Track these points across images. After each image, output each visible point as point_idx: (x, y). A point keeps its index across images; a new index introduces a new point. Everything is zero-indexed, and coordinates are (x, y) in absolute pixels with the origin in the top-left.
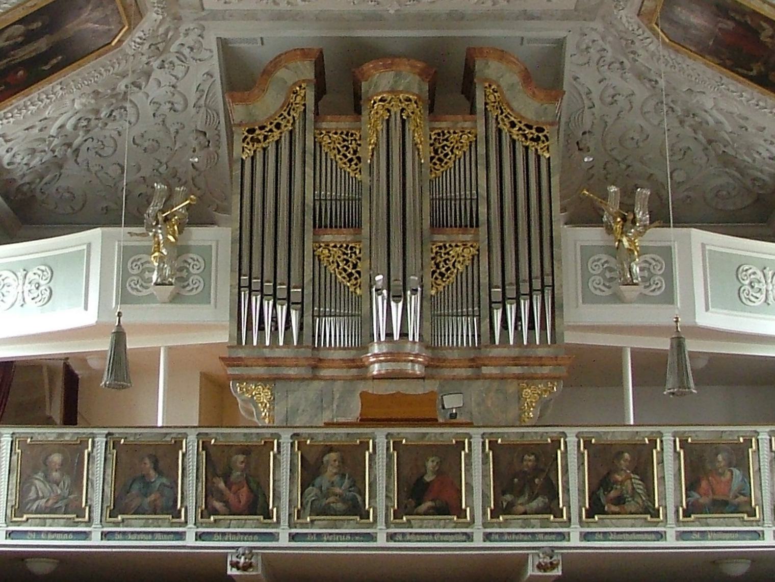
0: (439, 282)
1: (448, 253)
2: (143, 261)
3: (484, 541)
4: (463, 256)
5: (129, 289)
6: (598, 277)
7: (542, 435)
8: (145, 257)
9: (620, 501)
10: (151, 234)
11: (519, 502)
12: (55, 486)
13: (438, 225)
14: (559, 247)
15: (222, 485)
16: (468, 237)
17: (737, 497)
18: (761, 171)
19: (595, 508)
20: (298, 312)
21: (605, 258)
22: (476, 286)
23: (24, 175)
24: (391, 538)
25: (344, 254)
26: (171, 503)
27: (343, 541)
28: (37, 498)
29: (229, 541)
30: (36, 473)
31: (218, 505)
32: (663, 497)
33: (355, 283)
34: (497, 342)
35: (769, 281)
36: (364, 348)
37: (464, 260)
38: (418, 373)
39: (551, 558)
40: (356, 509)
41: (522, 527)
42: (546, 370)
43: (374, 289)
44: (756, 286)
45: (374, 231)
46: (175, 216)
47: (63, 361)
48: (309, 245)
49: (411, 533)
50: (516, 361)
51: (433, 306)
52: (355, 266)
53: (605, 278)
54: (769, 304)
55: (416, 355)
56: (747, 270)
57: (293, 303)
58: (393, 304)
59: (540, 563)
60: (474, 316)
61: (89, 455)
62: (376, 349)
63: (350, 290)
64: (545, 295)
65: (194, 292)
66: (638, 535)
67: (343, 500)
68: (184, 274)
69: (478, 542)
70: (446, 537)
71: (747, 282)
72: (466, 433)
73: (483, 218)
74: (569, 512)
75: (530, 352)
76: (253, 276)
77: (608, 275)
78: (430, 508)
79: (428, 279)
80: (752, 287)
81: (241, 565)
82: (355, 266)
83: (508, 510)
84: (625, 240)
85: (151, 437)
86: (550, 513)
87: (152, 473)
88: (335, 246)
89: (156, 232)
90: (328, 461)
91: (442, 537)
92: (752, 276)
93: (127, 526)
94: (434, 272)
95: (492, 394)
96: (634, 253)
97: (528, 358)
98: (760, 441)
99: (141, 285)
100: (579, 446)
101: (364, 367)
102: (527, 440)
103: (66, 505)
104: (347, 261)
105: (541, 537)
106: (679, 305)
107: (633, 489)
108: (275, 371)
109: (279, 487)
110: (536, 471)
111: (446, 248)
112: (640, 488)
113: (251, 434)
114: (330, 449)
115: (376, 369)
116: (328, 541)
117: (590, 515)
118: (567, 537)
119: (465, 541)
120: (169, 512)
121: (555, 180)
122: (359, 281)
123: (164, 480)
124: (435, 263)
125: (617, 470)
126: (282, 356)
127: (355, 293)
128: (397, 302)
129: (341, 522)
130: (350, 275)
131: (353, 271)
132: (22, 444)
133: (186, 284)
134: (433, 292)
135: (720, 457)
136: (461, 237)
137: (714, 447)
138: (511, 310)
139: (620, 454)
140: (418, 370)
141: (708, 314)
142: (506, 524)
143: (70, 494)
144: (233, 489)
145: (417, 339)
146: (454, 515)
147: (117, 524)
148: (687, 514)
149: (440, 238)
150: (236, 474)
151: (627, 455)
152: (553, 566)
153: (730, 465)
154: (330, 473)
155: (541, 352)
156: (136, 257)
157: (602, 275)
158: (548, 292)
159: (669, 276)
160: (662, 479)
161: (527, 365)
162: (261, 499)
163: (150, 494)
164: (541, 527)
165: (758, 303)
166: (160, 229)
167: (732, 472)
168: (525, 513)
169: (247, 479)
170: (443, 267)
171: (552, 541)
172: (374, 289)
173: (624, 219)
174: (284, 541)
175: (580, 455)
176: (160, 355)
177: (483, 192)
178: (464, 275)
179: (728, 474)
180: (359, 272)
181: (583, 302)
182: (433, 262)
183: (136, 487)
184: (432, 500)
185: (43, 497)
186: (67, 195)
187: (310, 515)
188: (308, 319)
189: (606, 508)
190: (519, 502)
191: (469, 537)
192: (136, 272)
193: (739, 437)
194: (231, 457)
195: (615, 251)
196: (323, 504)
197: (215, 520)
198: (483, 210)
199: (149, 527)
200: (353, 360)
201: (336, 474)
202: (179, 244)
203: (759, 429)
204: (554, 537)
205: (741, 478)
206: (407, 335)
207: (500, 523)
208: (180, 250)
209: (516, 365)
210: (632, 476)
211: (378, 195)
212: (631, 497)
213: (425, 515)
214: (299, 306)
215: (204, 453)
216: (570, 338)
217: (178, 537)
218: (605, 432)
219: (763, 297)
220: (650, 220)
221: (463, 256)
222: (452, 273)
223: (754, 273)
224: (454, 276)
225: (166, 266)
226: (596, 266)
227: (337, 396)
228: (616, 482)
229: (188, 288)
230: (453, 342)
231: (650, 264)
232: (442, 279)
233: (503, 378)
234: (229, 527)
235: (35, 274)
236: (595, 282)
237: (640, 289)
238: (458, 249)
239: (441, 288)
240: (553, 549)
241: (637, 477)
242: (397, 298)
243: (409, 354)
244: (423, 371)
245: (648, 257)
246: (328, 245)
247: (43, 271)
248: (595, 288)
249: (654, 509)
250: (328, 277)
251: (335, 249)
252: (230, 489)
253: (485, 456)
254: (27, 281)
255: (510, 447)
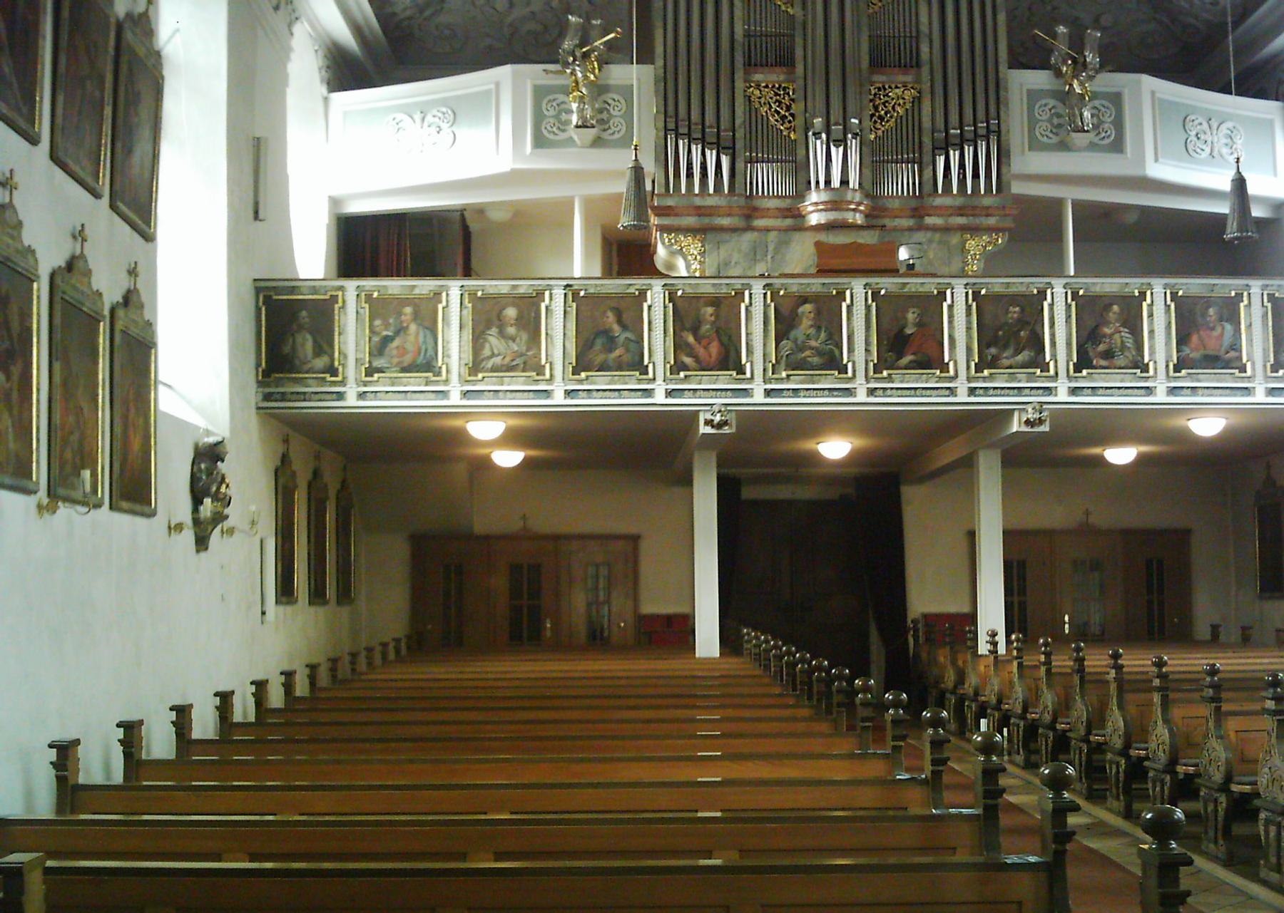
0: (878, 126)
1: (887, 95)
2: (558, 101)
3: (969, 396)
4: (904, 99)
5: (545, 132)
6: (1046, 124)
7: (1028, 285)
8: (561, 98)
9: (1108, 355)
10: (568, 71)
11: (1005, 355)
12: (511, 343)
13: (877, 63)
14: (1006, 90)
15: (691, 339)
16: (909, 78)
17: (1227, 352)
18: (1196, 18)
19: (1083, 362)
20: (728, 157)
21: (1052, 102)
22: (916, 128)
23: (405, 9)
24: (872, 394)
25: (776, 94)
26: (637, 358)
27: (821, 397)
28: (493, 355)
29: (700, 397)
30: (489, 328)
31: (688, 360)
32: (1152, 352)
33: (789, 126)
34: (940, 192)
35: (1215, 132)
36: (800, 196)
37: (904, 103)
38: (859, 222)
39: (1040, 413)
40: (833, 362)
41: (1007, 381)
42: (992, 221)
43: (810, 133)
44: (1202, 137)
45: (810, 66)
46: (594, 51)
47: (459, 213)
48: (740, 85)
49: (892, 389)
50: (960, 211)
51: (873, 153)
52: (788, 108)
53: (1052, 125)
54: (1213, 157)
55: (859, 204)
56: (1193, 121)
57: (708, 143)
58: (833, 149)
59: (1028, 419)
60: (914, 163)
61: (547, 307)
62: (814, 197)
63: (784, 133)
64: (991, 141)
65: (617, 136)
66: (1108, 391)
67: (819, 352)
68: (605, 116)
69: (962, 397)
70: (928, 392)
71: (1194, 133)
72: (948, 284)
73: (925, 55)
74: (1253, 369)
75: (975, 202)
76: (707, 123)
77: (1055, 121)
78: (911, 362)
79: (867, 123)
80: (1198, 138)
81: (715, 422)
82: (788, 108)
83: (993, 364)
84: (1075, 85)
85: (613, 289)
86: (1036, 368)
87: (616, 327)
88: (767, 87)
89: (574, 70)
90: (803, 313)
91: (924, 392)
92: (1199, 127)
93: (591, 384)
94: (872, 116)
95: (934, 245)
96: (1085, 98)
97: (974, 208)
98: (753, 295)
99: (559, 128)
100: (866, 300)
101: (800, 216)
102: (1013, 290)
103: (525, 363)
104: (780, 103)
105: (1027, 391)
106: (1129, 155)
107: (1122, 342)
108: (706, 220)
109: (752, 340)
110: (1022, 323)
111: (885, 89)
112: (1130, 342)
113: (721, 284)
114: (804, 300)
115: (814, 219)
116: (804, 397)
117: (1078, 369)
118: (1054, 392)
119: (949, 396)
120: (637, 368)
121: (1002, 18)
122: (793, 124)
123: (629, 335)
124: (874, 105)
125: (1107, 323)
126: (715, 205)
127: (789, 137)
128: (837, 147)
129: (818, 377)
130: (784, 117)
131: (787, 114)
132: (473, 295)
133: (607, 126)
134: (872, 137)
135: (1211, 311)
136: (901, 78)
137: (1207, 302)
138: (968, 152)
139: (1108, 307)
140: (859, 219)
141: (1157, 165)
142: (991, 377)
143: (528, 350)
144: (702, 344)
145: (857, 187)
146: (936, 369)
147: (580, 382)
148: (1177, 369)
149: (879, 78)
150: (706, 328)
151: (1115, 308)
152: (1041, 421)
153: (1221, 319)
154: (805, 325)
155: (987, 201)
156: (551, 97)
157: (1050, 120)
158: (993, 139)
159: (1119, 124)
160: (1151, 332)
161: (972, 216)
162: (733, 354)
163: (616, 349)
164: (1028, 382)
165: (1205, 155)
166: (578, 66)
167: (1223, 328)
168: (1010, 367)
169: (717, 332)
170: (882, 109)
171: (1038, 395)
172: (810, 133)
173: (1075, 61)
174: (759, 397)
175: (1068, 306)
176: (573, 205)
177: (924, 29)
178: (904, 119)
179: (1219, 330)
180: (792, 115)
181: (1029, 150)
182: (871, 104)
183: (599, 343)
184: (912, 354)
185: (499, 355)
186: (447, 32)
187: (785, 370)
188: (740, 165)
189: (1095, 362)
190: (1005, 355)
191: (952, 391)
192: (617, 120)
193: (1230, 290)
194: (700, 310)
195: (1064, 97)
196: (799, 358)
197: (686, 376)
198: (925, 49)
199: (615, 384)
200: (788, 210)
201: (812, 326)
202: (600, 82)
203: (1251, 282)
204: (1041, 392)
205: (1232, 333)
206: (848, 183)
207: (984, 378)
208: (599, 89)
209: (962, 215)
210: (1122, 329)
211: (814, 30)
212: (1120, 351)
213: (906, 369)
214: (731, 151)
215: (671, 305)
216: (1017, 188)
217: (646, 394)
218: (1094, 283)
219: (1208, 150)
220: (1100, 65)
221: (904, 99)
222: (891, 117)
223: (1201, 124)
224: (893, 120)
225: (586, 106)
226: (1043, 111)
227: (771, 248)
228: (1105, 336)
229: (610, 131)
230: (892, 192)
231: (1099, 111)
232: (881, 124)
233: (946, 229)
234: (700, 384)
235: (434, 116)
236: (1042, 128)
237: (1091, 136)
238: (897, 91)
239: (880, 133)
240: (1041, 403)
241: (1127, 330)
242: (838, 143)
243: (851, 202)
244: (864, 220)
245: (1097, 103)
246: (760, 86)
247: (444, 114)
248: (1043, 136)
249: (1143, 364)
250: (759, 121)
251: (766, 90)
252: (700, 343)
253: (969, 307)
254: (426, 123)
255: (995, 298)
